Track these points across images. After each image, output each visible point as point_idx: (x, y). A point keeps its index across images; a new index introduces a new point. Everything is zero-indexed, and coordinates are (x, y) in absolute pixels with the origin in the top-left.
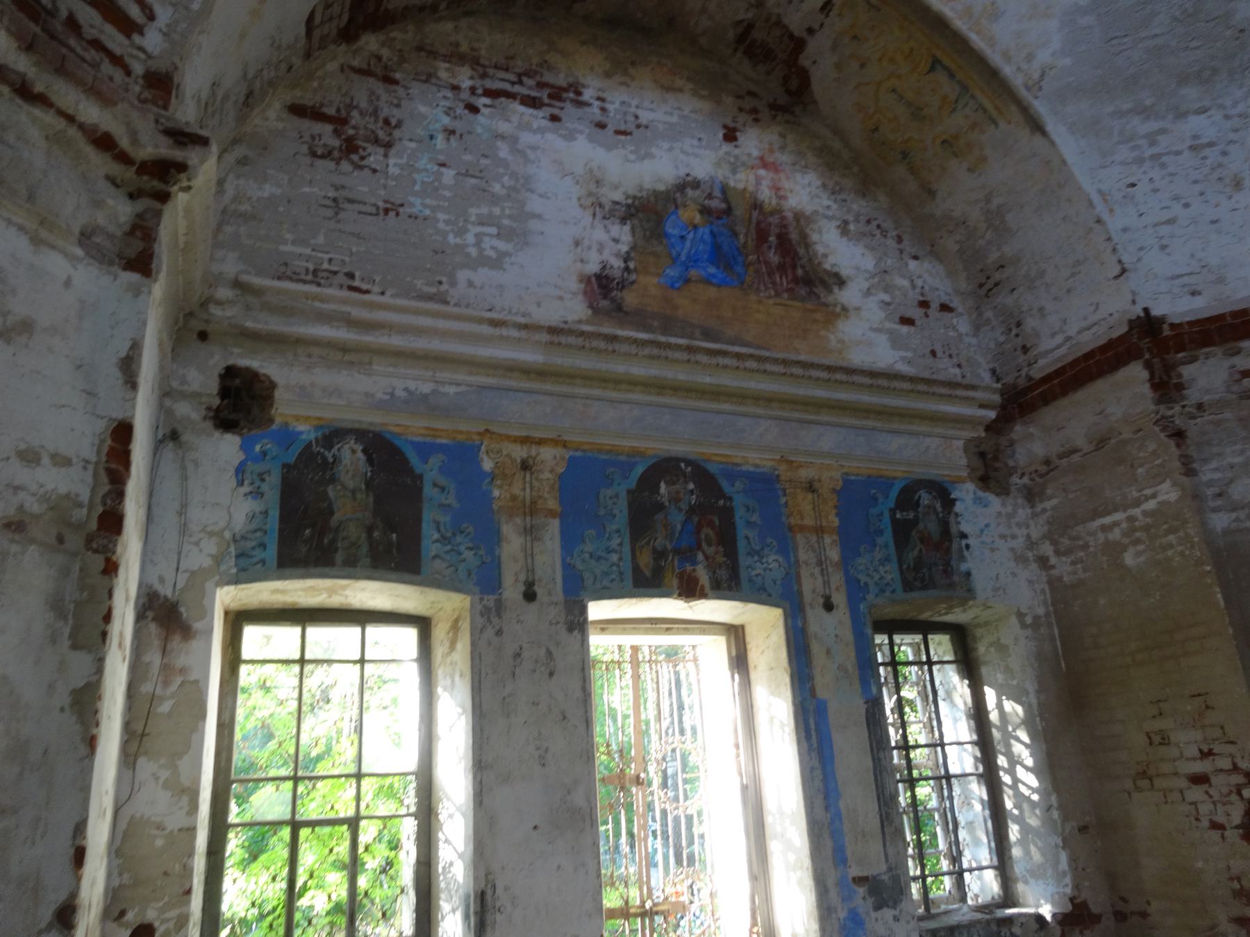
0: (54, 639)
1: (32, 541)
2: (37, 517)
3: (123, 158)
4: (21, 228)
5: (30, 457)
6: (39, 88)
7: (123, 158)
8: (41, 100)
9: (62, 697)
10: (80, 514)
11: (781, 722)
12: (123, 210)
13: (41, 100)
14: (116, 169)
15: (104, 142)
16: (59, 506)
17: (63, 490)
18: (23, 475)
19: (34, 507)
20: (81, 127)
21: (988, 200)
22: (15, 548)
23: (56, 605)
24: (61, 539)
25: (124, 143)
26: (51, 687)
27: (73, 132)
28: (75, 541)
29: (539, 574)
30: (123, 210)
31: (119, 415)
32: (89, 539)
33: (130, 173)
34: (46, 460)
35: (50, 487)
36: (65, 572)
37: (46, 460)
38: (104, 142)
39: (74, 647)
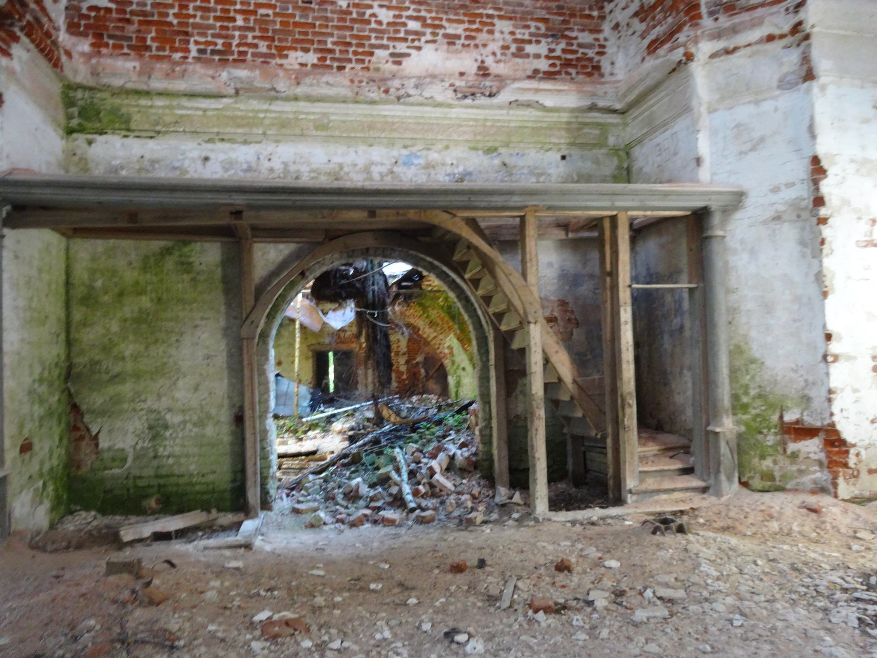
0: (804, 256)
1: (784, 222)
2: (784, 212)
3: (782, 36)
4: (750, 102)
5: (775, 190)
6: (732, 47)
7: (782, 36)
8: (735, 49)
9: (812, 278)
10: (804, 204)
11: (157, 621)
12: (793, 57)
13: (735, 49)
14: (785, 41)
15: (770, 38)
16: (795, 205)
17: (794, 197)
18: (774, 198)
19: (781, 208)
20: (756, 43)
21: (194, 280)
22: (778, 226)
23: (803, 243)
24: (799, 216)
25: (777, 32)
26: (807, 275)
27: (754, 48)
28: (805, 215)
29: (304, 516)
30: (793, 57)
31: (811, 154)
32: (811, 211)
33: (789, 40)
34: (783, 188)
35: (787, 198)
36: (803, 229)
37: (783, 188)
38: (770, 38)
39: (813, 257)
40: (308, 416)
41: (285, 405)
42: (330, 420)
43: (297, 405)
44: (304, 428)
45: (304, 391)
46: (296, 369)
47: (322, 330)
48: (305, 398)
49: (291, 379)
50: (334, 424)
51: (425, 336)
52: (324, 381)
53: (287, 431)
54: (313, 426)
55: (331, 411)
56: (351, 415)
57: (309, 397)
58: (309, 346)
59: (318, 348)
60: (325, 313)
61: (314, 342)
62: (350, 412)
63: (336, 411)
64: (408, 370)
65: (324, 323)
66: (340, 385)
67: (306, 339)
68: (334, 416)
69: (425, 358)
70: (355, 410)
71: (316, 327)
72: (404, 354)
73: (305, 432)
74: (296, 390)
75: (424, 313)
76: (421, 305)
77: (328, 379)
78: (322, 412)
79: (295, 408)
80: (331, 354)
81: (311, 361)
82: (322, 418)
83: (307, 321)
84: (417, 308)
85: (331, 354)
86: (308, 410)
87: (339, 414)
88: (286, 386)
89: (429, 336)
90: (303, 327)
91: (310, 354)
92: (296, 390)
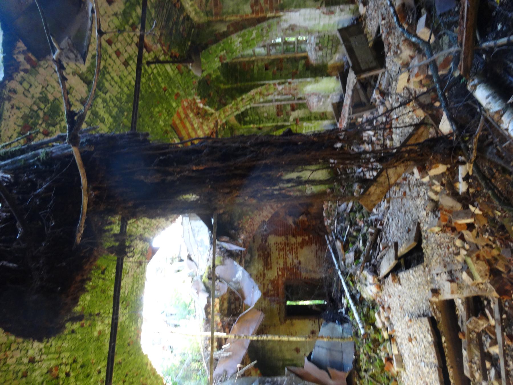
40: (354, 326)
41: (342, 352)
42: (359, 301)
43: (343, 338)
44: (371, 331)
45: (325, 330)
46: (303, 339)
47: (263, 310)
48: (333, 329)
49: (312, 345)
50: (365, 296)
51: (270, 216)
52: (314, 308)
53: (375, 352)
54: (368, 321)
55: (347, 300)
56: (351, 278)
57: (331, 324)
58: (282, 323)
59: (283, 315)
60: (247, 307)
61: (278, 318)
62: (348, 278)
63: (347, 294)
64: (301, 235)
65: (254, 307)
66: (316, 292)
67: (275, 325)
68: (353, 297)
69: (290, 216)
70: (344, 274)
71: (259, 317)
72: (287, 239)
73: (377, 331)
74: (325, 340)
75: (248, 215)
76: (240, 217)
77: (311, 306)
78: (348, 310)
79: (345, 340)
80: (288, 303)
81: (294, 321)
82: (357, 310)
83: (254, 326)
84: (244, 220)
85: (288, 303)
86: (346, 325)
87: (350, 291)
88: (321, 349)
89: (270, 213)
90: (260, 331)
91: (288, 322)
92: (325, 340)
